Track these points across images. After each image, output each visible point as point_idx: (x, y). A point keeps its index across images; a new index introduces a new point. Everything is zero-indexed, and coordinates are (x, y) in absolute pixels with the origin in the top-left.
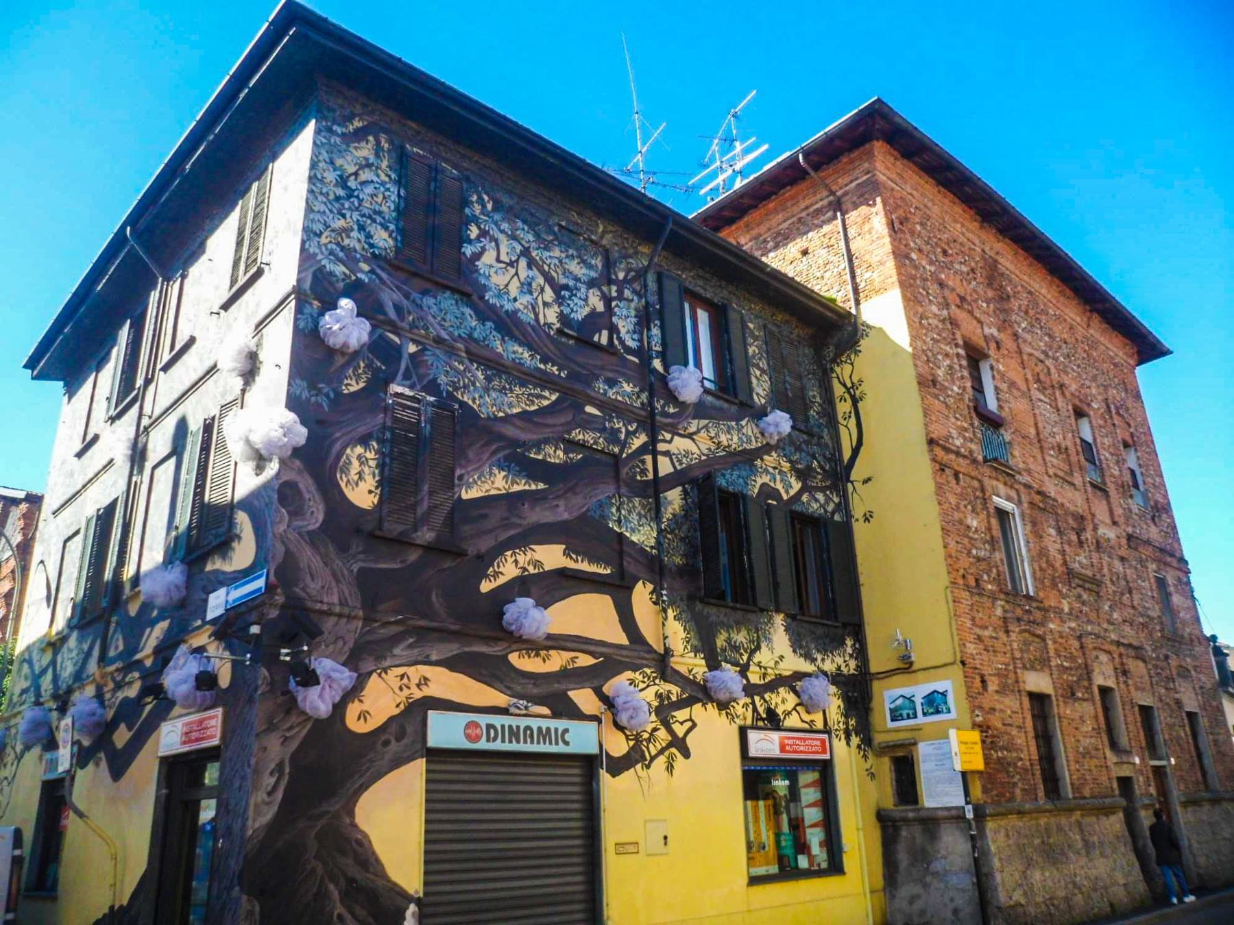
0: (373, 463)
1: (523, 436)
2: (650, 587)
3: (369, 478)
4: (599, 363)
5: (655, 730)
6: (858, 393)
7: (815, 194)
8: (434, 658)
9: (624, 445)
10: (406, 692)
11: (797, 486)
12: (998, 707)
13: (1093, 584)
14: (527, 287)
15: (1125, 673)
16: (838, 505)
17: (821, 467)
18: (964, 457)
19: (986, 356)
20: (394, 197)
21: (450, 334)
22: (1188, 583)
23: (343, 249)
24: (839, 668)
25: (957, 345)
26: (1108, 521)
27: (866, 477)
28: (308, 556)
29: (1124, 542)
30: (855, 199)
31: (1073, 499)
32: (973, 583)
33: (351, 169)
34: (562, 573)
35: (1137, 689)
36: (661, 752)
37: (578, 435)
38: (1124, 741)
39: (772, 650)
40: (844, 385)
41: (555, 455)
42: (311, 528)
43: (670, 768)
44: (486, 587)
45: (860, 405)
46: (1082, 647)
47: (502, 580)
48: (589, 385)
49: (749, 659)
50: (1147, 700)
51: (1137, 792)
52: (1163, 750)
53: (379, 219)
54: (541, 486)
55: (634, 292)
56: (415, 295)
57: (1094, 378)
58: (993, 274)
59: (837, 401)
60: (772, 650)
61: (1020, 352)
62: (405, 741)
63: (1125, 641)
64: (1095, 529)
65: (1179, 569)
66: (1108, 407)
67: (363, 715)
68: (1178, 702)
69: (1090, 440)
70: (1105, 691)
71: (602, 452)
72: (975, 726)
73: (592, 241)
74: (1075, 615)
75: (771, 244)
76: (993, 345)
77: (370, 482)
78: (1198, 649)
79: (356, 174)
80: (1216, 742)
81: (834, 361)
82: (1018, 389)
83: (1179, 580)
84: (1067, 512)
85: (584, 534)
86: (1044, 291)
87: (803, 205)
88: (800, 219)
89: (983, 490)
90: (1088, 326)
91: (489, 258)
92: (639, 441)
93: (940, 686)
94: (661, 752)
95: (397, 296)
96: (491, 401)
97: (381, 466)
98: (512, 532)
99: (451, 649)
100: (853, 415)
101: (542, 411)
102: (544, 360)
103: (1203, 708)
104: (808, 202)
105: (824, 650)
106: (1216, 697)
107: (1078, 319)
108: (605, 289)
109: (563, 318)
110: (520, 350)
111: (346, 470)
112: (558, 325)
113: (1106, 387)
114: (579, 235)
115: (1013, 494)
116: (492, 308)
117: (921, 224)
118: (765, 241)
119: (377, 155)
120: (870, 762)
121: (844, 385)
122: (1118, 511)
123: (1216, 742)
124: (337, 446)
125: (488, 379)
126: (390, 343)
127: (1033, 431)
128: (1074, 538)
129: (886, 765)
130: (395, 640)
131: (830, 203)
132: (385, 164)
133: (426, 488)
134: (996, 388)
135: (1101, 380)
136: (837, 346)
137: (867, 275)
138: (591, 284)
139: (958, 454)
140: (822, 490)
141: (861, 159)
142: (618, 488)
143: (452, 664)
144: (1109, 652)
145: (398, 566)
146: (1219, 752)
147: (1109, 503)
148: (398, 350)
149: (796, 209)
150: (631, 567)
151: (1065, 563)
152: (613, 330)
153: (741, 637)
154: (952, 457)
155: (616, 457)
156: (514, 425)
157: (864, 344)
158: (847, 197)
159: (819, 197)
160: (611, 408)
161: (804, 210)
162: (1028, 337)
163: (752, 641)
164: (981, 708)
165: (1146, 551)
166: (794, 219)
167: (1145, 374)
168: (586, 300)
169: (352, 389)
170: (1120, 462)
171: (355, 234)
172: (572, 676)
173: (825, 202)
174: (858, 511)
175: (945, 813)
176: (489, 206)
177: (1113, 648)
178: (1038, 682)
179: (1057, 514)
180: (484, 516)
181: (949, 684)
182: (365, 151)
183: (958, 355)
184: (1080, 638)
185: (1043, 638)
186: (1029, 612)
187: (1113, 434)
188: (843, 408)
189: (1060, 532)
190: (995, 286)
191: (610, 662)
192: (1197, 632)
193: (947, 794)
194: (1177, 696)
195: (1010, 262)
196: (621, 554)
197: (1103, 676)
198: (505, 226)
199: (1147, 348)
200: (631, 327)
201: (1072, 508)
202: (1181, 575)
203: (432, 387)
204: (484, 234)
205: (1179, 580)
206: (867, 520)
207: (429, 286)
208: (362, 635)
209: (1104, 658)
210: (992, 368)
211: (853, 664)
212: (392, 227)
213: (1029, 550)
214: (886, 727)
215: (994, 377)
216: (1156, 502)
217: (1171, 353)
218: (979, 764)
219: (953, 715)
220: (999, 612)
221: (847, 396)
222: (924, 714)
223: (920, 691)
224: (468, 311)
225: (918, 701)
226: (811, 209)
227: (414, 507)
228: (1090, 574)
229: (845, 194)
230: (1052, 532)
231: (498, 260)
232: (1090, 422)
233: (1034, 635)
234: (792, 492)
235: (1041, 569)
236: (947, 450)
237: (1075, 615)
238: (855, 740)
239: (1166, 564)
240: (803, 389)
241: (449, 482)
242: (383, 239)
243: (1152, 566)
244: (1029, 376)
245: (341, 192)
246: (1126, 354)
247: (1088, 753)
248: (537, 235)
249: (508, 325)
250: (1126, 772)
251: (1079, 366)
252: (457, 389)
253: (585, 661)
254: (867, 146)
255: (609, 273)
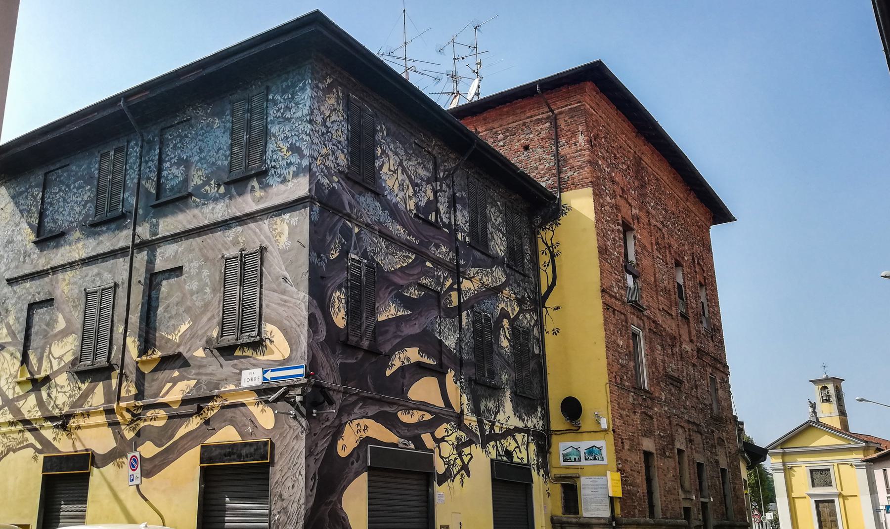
0: (343, 301)
1: (401, 282)
2: (453, 372)
3: (342, 310)
4: (431, 234)
5: (456, 459)
6: (555, 250)
7: (538, 108)
8: (370, 414)
9: (442, 285)
10: (360, 434)
11: (517, 309)
12: (629, 459)
13: (676, 382)
14: (402, 187)
15: (691, 441)
16: (536, 321)
17: (529, 297)
18: (618, 299)
19: (632, 229)
20: (346, 131)
21: (371, 220)
22: (727, 382)
23: (326, 167)
24: (534, 426)
25: (618, 224)
26: (687, 339)
27: (556, 305)
28: (321, 357)
29: (695, 353)
30: (567, 118)
31: (670, 325)
32: (619, 381)
33: (327, 114)
34: (419, 365)
35: (696, 452)
36: (458, 473)
37: (424, 281)
38: (687, 484)
39: (504, 412)
40: (546, 244)
41: (414, 293)
42: (321, 340)
43: (462, 482)
44: (388, 373)
45: (556, 259)
46: (670, 424)
47: (395, 368)
48: (428, 248)
49: (495, 418)
50: (700, 459)
51: (693, 517)
52: (706, 492)
53: (340, 147)
54: (409, 312)
55: (448, 186)
56: (357, 196)
57: (686, 239)
58: (638, 167)
59: (540, 253)
60: (504, 412)
61: (649, 223)
62: (360, 462)
63: (692, 420)
64: (681, 345)
65: (723, 372)
66: (693, 259)
67: (344, 447)
68: (717, 462)
69: (682, 284)
70: (680, 452)
71: (433, 290)
72: (618, 470)
73: (428, 152)
74: (667, 402)
75: (501, 136)
76: (636, 221)
77: (342, 313)
78: (730, 427)
79: (329, 116)
80: (734, 488)
81: (540, 226)
82: (647, 251)
83: (723, 379)
84: (668, 334)
85: (427, 341)
86: (665, 178)
87: (528, 115)
88: (524, 124)
89: (626, 322)
90: (687, 200)
91: (385, 169)
92: (449, 282)
93: (598, 443)
94: (458, 473)
95: (349, 197)
96: (393, 261)
97: (347, 303)
98: (398, 340)
99: (373, 410)
100: (550, 264)
101: (410, 266)
102: (409, 235)
103: (729, 466)
104: (532, 113)
105: (529, 414)
106: (736, 459)
107: (682, 196)
108: (434, 184)
109: (417, 205)
110: (399, 227)
111: (333, 307)
112: (415, 211)
113: (692, 244)
114: (423, 148)
115: (641, 323)
116: (388, 201)
117: (605, 138)
118: (496, 133)
119: (338, 103)
120: (548, 485)
121: (546, 244)
122: (694, 332)
123: (734, 488)
124: (329, 292)
125: (387, 247)
126: (347, 227)
127: (653, 279)
128: (670, 351)
129: (557, 489)
130: (355, 404)
131: (549, 117)
132: (341, 108)
133: (364, 315)
134: (636, 252)
135: (690, 240)
136: (543, 218)
137: (570, 174)
138: (428, 181)
139: (615, 298)
140: (529, 311)
141: (576, 92)
142: (440, 312)
143: (376, 418)
144: (683, 427)
145: (354, 361)
146: (735, 495)
147: (689, 327)
148: (351, 230)
149: (523, 116)
150: (445, 361)
151: (664, 368)
152: (437, 212)
153: (491, 405)
154: (613, 300)
155: (438, 293)
156: (398, 276)
157: (563, 219)
158: (562, 116)
159: (541, 111)
160: (437, 262)
161: (528, 118)
162: (654, 212)
163: (496, 407)
164: (621, 459)
165: (707, 359)
166: (521, 122)
167: (717, 232)
168: (425, 193)
169: (334, 257)
170: (697, 298)
171: (330, 157)
172: (422, 425)
173: (545, 116)
174: (549, 326)
175: (597, 521)
176: (385, 133)
177: (685, 425)
178: (648, 444)
179: (662, 336)
180: (387, 332)
181: (605, 445)
182: (332, 101)
183: (618, 230)
184: (669, 417)
185: (651, 417)
186: (645, 400)
187: (693, 278)
188: (544, 259)
189: (662, 346)
190: (639, 177)
191: (438, 418)
192: (729, 415)
193: (598, 509)
194: (716, 458)
195: (649, 159)
196: (441, 352)
197: (680, 444)
198: (392, 146)
199: (721, 215)
200: (445, 209)
201: (670, 331)
202: (724, 375)
203: (365, 255)
204: (383, 152)
205: (723, 379)
206: (554, 333)
207: (361, 189)
208: (343, 401)
209: (680, 431)
210: (635, 237)
211: (541, 423)
212: (346, 151)
213: (647, 360)
214: (557, 460)
215: (635, 244)
216: (714, 325)
217: (734, 220)
218: (619, 494)
219: (605, 462)
220: (631, 400)
221: (547, 251)
222: (586, 460)
223: (584, 445)
224: (378, 204)
225: (583, 451)
226: (534, 118)
227: (360, 326)
228: (676, 375)
229: (561, 113)
230: (659, 347)
231: (390, 170)
232: (683, 271)
233: (647, 415)
234: (515, 313)
235: (653, 373)
236: (611, 296)
237: (667, 402)
238: (542, 472)
239: (717, 369)
240: (522, 245)
241: (373, 312)
242: (343, 160)
243: (709, 370)
244: (654, 242)
245: (324, 130)
246: (706, 218)
247: (670, 491)
248: (406, 151)
249: (394, 211)
250: (686, 504)
251: (679, 231)
252: (375, 254)
253: (428, 417)
254: (582, 84)
255: (436, 174)
